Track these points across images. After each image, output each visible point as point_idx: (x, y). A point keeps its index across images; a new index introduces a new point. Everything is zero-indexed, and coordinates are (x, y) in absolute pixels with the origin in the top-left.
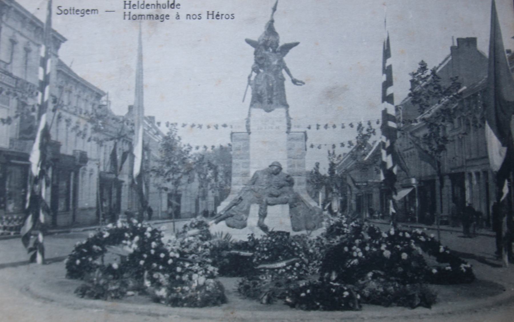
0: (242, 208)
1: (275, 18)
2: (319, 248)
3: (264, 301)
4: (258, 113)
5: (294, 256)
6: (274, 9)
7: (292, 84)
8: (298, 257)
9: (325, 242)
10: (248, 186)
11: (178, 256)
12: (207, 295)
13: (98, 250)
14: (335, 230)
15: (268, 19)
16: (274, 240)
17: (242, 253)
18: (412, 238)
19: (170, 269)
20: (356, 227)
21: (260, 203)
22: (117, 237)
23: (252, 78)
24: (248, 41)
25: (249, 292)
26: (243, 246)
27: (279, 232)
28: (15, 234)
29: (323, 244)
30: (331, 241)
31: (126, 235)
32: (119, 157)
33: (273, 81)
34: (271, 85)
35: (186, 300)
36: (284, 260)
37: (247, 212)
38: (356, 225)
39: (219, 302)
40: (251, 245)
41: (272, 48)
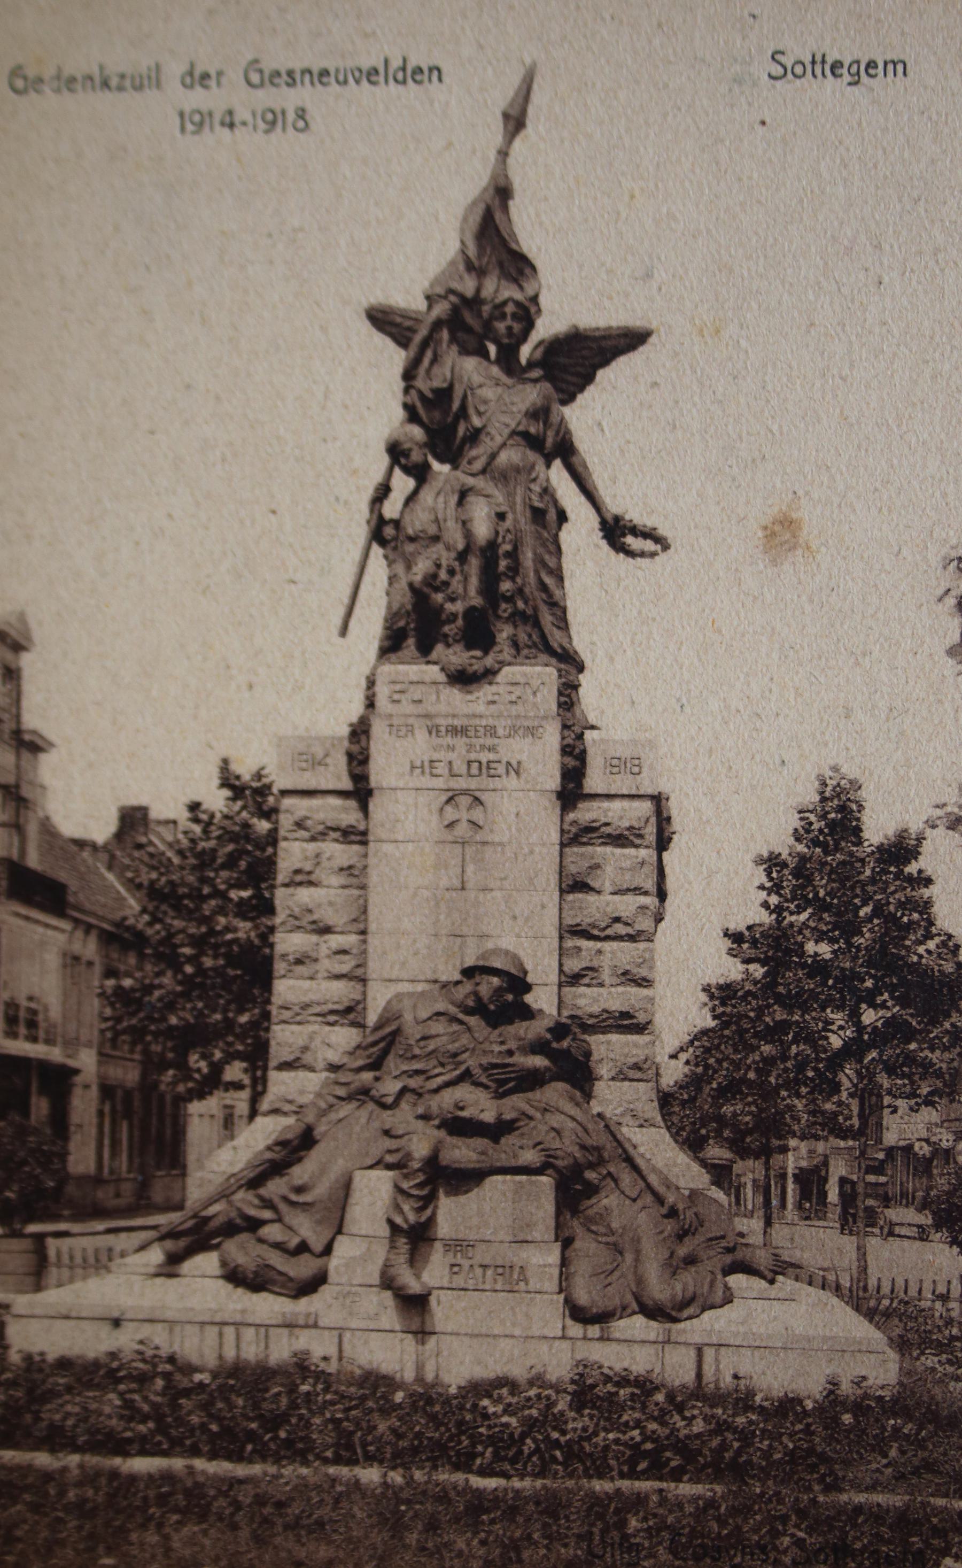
6: (515, 122)
24: (383, 319)
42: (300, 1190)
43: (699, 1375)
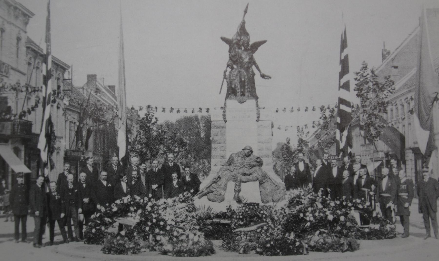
0: (220, 185)
1: (246, 20)
2: (282, 216)
3: (241, 252)
4: (232, 103)
5: (263, 222)
6: (246, 12)
7: (261, 78)
8: (266, 222)
9: (287, 211)
10: (225, 167)
11: (173, 223)
12: (200, 248)
13: (108, 221)
14: (295, 202)
15: (241, 20)
16: (247, 210)
17: (223, 221)
18: (353, 206)
19: (169, 233)
20: (311, 199)
21: (235, 181)
22: (124, 211)
23: (227, 73)
24: (223, 39)
25: (231, 247)
26: (223, 216)
27: (250, 204)
28: (4, 213)
29: (285, 213)
30: (292, 211)
31: (132, 209)
32: (84, 133)
33: (245, 76)
34: (243, 79)
35: (186, 252)
36: (255, 225)
37: (225, 189)
38: (312, 197)
39: (210, 253)
40: (228, 214)
41: (244, 46)
42: (219, 186)
43: (17, 95)
